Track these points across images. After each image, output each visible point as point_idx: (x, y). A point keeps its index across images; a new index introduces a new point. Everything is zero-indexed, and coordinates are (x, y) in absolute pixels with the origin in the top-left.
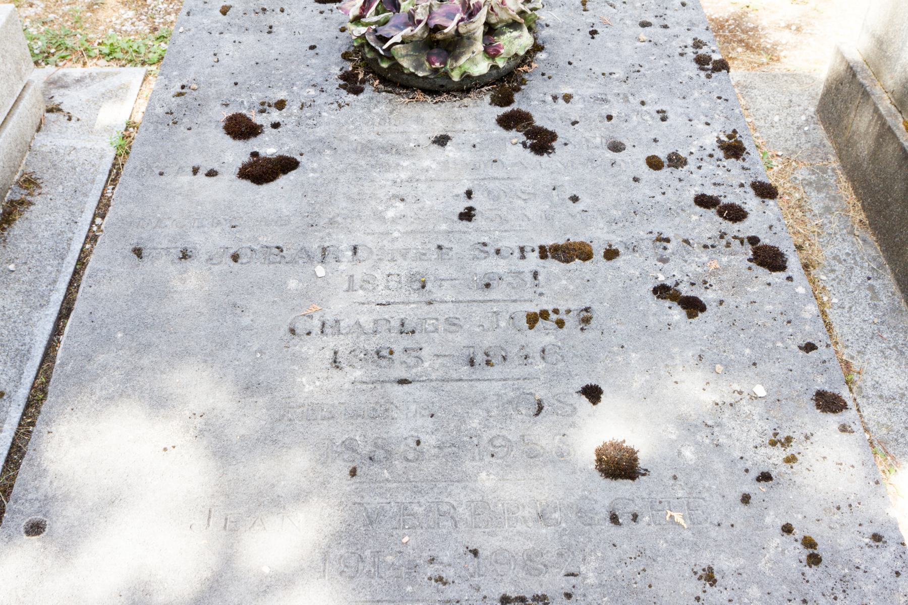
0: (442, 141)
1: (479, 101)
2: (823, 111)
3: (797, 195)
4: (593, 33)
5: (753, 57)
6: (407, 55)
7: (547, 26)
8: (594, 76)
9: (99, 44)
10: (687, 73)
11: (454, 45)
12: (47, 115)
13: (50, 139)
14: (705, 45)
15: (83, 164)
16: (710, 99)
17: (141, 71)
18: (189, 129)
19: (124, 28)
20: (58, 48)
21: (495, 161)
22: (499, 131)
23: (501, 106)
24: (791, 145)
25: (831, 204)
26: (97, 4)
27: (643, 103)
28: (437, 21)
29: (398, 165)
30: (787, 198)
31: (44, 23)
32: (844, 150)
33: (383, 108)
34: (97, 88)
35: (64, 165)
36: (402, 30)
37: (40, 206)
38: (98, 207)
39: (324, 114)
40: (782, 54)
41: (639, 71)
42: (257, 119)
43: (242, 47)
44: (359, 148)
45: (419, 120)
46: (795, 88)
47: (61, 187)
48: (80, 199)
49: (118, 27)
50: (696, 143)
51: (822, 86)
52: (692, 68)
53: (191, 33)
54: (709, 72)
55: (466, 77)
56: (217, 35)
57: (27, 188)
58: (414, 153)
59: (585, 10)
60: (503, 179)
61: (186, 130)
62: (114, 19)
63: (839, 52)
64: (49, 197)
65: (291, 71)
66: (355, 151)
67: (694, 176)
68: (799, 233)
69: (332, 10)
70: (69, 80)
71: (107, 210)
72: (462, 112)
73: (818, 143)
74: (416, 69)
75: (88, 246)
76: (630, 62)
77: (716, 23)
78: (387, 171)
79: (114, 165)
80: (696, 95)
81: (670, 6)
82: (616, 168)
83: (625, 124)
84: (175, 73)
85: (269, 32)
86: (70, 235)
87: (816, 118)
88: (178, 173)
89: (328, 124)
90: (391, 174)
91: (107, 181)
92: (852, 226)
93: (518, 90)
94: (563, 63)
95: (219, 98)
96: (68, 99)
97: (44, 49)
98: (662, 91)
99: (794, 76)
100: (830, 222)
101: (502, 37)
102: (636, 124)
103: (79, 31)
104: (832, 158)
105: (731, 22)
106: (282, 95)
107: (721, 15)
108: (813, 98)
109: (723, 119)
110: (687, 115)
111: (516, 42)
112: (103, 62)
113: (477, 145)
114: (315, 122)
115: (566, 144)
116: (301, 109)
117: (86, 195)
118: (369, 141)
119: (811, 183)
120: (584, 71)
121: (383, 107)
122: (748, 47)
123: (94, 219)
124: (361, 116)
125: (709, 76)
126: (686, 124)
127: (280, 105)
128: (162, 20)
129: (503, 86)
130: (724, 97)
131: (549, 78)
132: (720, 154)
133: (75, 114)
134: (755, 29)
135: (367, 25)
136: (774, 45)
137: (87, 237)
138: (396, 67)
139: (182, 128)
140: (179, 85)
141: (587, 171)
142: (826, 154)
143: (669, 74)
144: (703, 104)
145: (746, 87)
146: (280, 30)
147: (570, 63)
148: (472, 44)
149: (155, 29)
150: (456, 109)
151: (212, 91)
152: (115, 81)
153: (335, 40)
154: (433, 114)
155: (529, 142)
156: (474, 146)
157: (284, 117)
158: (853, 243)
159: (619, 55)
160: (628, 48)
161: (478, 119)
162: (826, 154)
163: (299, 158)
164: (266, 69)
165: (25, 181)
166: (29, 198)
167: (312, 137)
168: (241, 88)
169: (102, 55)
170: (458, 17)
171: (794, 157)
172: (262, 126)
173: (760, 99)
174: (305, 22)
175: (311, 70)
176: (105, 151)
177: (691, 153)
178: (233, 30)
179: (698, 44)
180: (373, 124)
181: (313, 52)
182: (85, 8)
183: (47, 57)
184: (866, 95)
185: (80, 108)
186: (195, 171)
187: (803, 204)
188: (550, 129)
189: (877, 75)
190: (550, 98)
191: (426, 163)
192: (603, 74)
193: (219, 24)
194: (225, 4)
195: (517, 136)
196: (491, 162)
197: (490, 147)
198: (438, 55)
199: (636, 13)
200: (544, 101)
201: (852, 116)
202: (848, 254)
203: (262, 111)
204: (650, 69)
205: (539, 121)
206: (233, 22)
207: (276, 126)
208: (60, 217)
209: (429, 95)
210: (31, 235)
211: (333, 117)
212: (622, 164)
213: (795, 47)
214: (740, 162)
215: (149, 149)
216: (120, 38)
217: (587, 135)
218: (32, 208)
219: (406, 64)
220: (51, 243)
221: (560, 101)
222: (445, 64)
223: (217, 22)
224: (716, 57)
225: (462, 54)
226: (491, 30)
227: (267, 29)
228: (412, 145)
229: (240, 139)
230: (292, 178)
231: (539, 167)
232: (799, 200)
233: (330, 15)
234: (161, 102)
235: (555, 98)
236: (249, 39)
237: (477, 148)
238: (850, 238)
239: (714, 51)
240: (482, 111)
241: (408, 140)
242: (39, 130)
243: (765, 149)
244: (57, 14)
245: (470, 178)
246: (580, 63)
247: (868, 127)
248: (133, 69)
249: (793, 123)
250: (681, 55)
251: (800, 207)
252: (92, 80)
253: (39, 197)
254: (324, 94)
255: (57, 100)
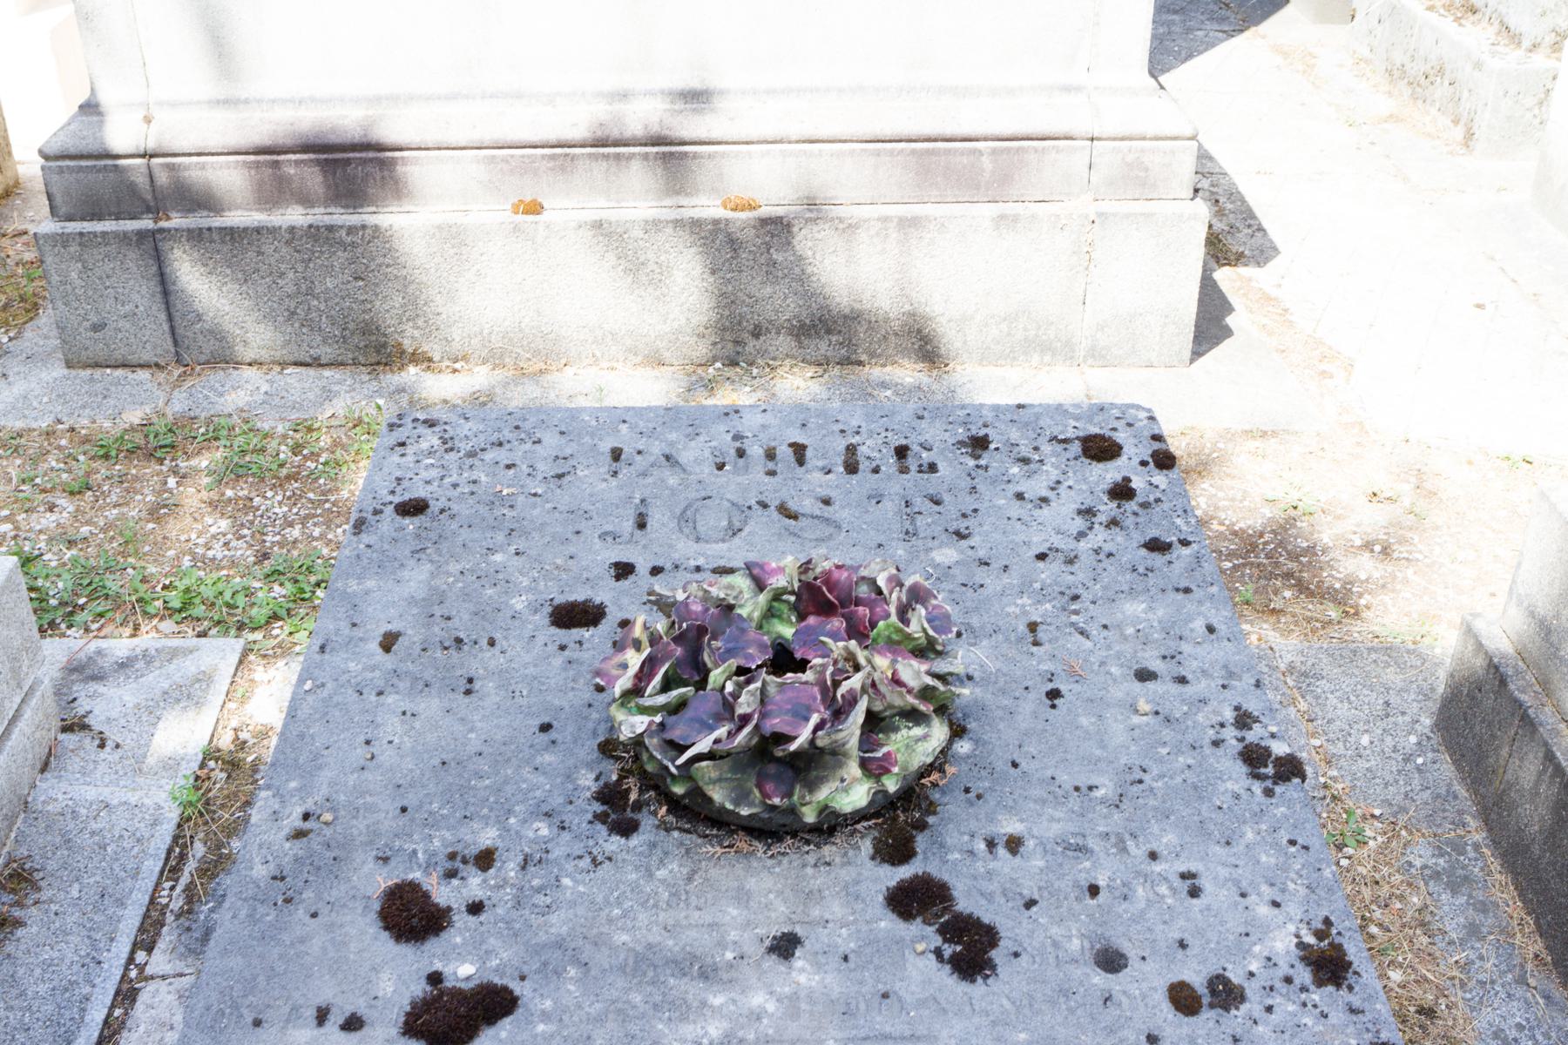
0: (785, 946)
1: (851, 853)
2: (1446, 729)
3: (1415, 900)
4: (1054, 694)
5: (1313, 608)
6: (720, 780)
7: (970, 678)
8: (1060, 792)
9: (165, 587)
10: (1229, 785)
11: (810, 765)
12: (61, 737)
13: (64, 786)
14: (1257, 720)
15: (121, 836)
16: (1276, 845)
17: (232, 646)
18: (314, 915)
19: (210, 554)
20: (91, 598)
21: (885, 996)
22: (889, 923)
23: (893, 864)
24: (1395, 794)
25: (1479, 918)
26: (165, 506)
27: (1153, 856)
28: (775, 724)
29: (704, 1004)
30: (1398, 906)
31: (71, 543)
32: (1494, 810)
33: (673, 869)
34: (156, 680)
35: (86, 840)
36: (712, 729)
37: (34, 929)
38: (142, 929)
39: (566, 881)
40: (1363, 602)
41: (1140, 782)
42: (443, 894)
43: (417, 725)
44: (631, 961)
45: (742, 897)
46: (1392, 676)
47: (76, 886)
48: (110, 912)
49: (200, 551)
50: (1257, 949)
51: (1442, 674)
52: (1235, 776)
53: (325, 693)
54: (1269, 783)
55: (825, 810)
56: (373, 698)
57: (13, 891)
58: (733, 974)
59: (1036, 643)
60: (903, 1038)
61: (307, 919)
62: (193, 536)
63: (1469, 631)
64: (54, 907)
65: (506, 782)
66: (622, 969)
67: (1260, 1028)
68: (1426, 980)
69: (580, 643)
70: (105, 663)
71: (158, 934)
72: (817, 879)
73: (1443, 791)
74: (737, 803)
75: (117, 1012)
76: (1124, 760)
77: (1241, 539)
78: (684, 1019)
79: (176, 838)
80: (1250, 835)
81: (1186, 633)
82: (1113, 1011)
83: (1125, 905)
84: (293, 784)
85: (468, 692)
86: (87, 990)
87: (1436, 739)
88: (288, 1021)
89: (573, 904)
90: (691, 1027)
91: (162, 873)
92: (1522, 966)
93: (922, 826)
94: (1001, 765)
95: (371, 842)
96: (106, 704)
97: (66, 597)
98: (1187, 828)
99: (1388, 650)
100: (1481, 958)
101: (893, 737)
102: (1142, 905)
103: (130, 560)
104: (1473, 823)
105: (1267, 537)
106: (487, 837)
107: (1249, 522)
108: (1427, 698)
109: (1303, 891)
110: (1237, 883)
111: (916, 745)
112: (168, 625)
113: (852, 957)
114: (548, 900)
115: (1016, 955)
116: (523, 868)
117: (121, 903)
118: (650, 946)
119: (1438, 873)
120: (1041, 781)
121: (675, 866)
122: (1302, 588)
123: (133, 952)
124: (636, 887)
125: (1269, 793)
126: (1236, 904)
127: (485, 859)
128: (278, 538)
129: (895, 819)
130: (1300, 841)
131: (979, 797)
132: (1304, 975)
133: (113, 736)
134: (1311, 550)
135: (644, 710)
136: (1349, 582)
137: (117, 993)
138: (697, 793)
139: (301, 911)
140: (299, 811)
141: (1060, 1019)
142: (1461, 813)
143: (1195, 788)
144: (1264, 859)
145: (1305, 675)
146: (485, 686)
147: (1015, 765)
148: (840, 765)
149: (266, 556)
150: (809, 871)
151: (360, 826)
152: (188, 667)
153: (586, 711)
154: (767, 882)
155: (948, 950)
156: (846, 959)
157: (492, 888)
158: (1527, 1002)
159: (1103, 745)
160: (1117, 731)
161: (851, 894)
162: (1461, 813)
163: (516, 988)
164: (460, 776)
165: (11, 876)
166: (17, 912)
167: (543, 937)
168: (412, 820)
169: (169, 612)
170: (815, 719)
171: (1402, 819)
172: (449, 909)
173: (1332, 700)
174: (531, 670)
175: (542, 779)
176: (160, 802)
177: (1252, 974)
178: (401, 685)
179: (1244, 720)
180: (655, 906)
181: (544, 737)
182: (144, 514)
183: (71, 613)
184: (1528, 724)
185: (123, 722)
186: (322, 1016)
187: (1428, 918)
188: (986, 920)
189: (1545, 685)
190: (982, 846)
191: (758, 999)
192: (1077, 789)
193: (377, 673)
194: (390, 627)
195: (922, 935)
196: (877, 999)
197: (876, 961)
198: (778, 778)
199: (1127, 648)
200: (971, 852)
201: (1505, 752)
202: (1520, 1027)
203: (451, 874)
204: (1161, 776)
205: (965, 902)
206: (403, 667)
207: (475, 908)
208: (71, 950)
209: (758, 838)
210: (15, 992)
211: (581, 888)
212: (1124, 1000)
213: (1383, 586)
214: (1343, 992)
215: (236, 962)
216: (202, 573)
217: (1055, 931)
218: (20, 932)
219: (718, 795)
220: (49, 1008)
221: (1001, 851)
222: (789, 795)
223: (373, 668)
224: (1279, 749)
225: (821, 781)
226: (875, 723)
227: (462, 685)
228: (729, 955)
229: (408, 940)
230: (503, 1034)
231: (968, 1009)
232: (1420, 911)
233: (576, 655)
234: (264, 851)
235: (991, 844)
236: (430, 706)
237: (851, 965)
238: (1519, 991)
239: (1273, 736)
240: (859, 877)
241: (722, 945)
242: (45, 768)
243: (1350, 803)
244: (95, 524)
245: (840, 1035)
246: (1034, 765)
247: (1537, 783)
248: (221, 641)
249: (1395, 750)
250: (1216, 743)
251: (1423, 924)
252: (148, 663)
253: (34, 910)
254: (566, 836)
255: (83, 706)
